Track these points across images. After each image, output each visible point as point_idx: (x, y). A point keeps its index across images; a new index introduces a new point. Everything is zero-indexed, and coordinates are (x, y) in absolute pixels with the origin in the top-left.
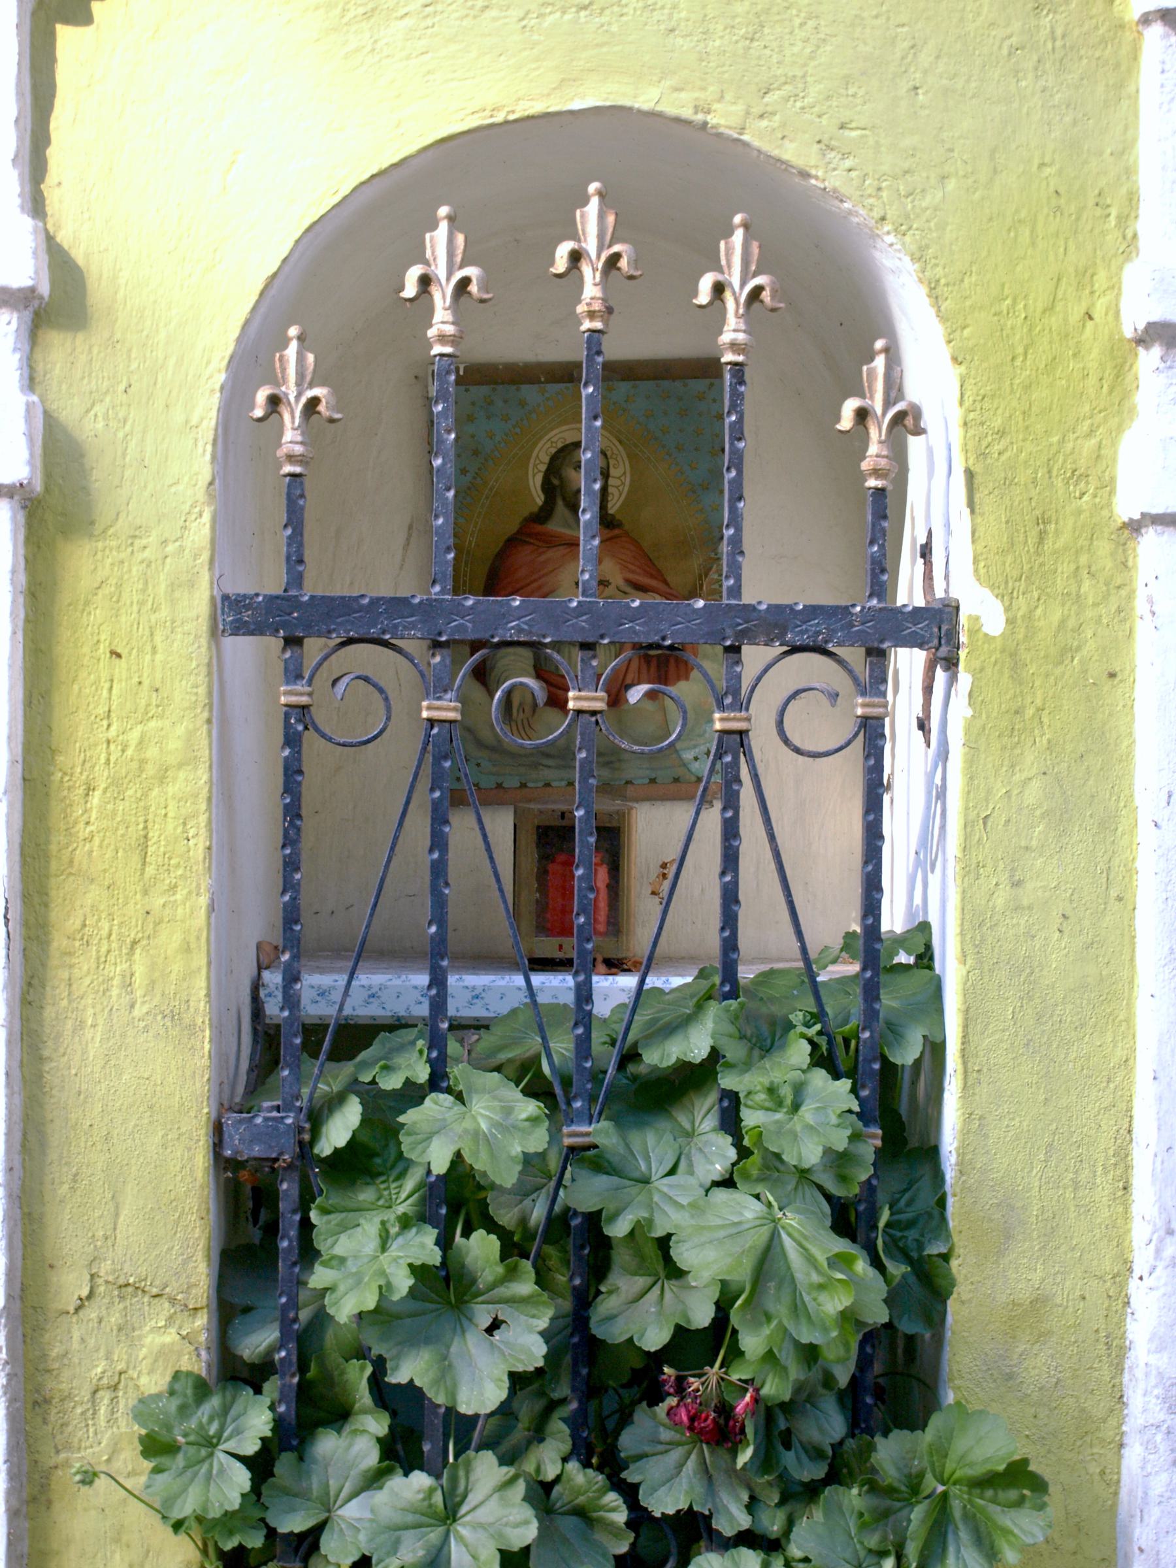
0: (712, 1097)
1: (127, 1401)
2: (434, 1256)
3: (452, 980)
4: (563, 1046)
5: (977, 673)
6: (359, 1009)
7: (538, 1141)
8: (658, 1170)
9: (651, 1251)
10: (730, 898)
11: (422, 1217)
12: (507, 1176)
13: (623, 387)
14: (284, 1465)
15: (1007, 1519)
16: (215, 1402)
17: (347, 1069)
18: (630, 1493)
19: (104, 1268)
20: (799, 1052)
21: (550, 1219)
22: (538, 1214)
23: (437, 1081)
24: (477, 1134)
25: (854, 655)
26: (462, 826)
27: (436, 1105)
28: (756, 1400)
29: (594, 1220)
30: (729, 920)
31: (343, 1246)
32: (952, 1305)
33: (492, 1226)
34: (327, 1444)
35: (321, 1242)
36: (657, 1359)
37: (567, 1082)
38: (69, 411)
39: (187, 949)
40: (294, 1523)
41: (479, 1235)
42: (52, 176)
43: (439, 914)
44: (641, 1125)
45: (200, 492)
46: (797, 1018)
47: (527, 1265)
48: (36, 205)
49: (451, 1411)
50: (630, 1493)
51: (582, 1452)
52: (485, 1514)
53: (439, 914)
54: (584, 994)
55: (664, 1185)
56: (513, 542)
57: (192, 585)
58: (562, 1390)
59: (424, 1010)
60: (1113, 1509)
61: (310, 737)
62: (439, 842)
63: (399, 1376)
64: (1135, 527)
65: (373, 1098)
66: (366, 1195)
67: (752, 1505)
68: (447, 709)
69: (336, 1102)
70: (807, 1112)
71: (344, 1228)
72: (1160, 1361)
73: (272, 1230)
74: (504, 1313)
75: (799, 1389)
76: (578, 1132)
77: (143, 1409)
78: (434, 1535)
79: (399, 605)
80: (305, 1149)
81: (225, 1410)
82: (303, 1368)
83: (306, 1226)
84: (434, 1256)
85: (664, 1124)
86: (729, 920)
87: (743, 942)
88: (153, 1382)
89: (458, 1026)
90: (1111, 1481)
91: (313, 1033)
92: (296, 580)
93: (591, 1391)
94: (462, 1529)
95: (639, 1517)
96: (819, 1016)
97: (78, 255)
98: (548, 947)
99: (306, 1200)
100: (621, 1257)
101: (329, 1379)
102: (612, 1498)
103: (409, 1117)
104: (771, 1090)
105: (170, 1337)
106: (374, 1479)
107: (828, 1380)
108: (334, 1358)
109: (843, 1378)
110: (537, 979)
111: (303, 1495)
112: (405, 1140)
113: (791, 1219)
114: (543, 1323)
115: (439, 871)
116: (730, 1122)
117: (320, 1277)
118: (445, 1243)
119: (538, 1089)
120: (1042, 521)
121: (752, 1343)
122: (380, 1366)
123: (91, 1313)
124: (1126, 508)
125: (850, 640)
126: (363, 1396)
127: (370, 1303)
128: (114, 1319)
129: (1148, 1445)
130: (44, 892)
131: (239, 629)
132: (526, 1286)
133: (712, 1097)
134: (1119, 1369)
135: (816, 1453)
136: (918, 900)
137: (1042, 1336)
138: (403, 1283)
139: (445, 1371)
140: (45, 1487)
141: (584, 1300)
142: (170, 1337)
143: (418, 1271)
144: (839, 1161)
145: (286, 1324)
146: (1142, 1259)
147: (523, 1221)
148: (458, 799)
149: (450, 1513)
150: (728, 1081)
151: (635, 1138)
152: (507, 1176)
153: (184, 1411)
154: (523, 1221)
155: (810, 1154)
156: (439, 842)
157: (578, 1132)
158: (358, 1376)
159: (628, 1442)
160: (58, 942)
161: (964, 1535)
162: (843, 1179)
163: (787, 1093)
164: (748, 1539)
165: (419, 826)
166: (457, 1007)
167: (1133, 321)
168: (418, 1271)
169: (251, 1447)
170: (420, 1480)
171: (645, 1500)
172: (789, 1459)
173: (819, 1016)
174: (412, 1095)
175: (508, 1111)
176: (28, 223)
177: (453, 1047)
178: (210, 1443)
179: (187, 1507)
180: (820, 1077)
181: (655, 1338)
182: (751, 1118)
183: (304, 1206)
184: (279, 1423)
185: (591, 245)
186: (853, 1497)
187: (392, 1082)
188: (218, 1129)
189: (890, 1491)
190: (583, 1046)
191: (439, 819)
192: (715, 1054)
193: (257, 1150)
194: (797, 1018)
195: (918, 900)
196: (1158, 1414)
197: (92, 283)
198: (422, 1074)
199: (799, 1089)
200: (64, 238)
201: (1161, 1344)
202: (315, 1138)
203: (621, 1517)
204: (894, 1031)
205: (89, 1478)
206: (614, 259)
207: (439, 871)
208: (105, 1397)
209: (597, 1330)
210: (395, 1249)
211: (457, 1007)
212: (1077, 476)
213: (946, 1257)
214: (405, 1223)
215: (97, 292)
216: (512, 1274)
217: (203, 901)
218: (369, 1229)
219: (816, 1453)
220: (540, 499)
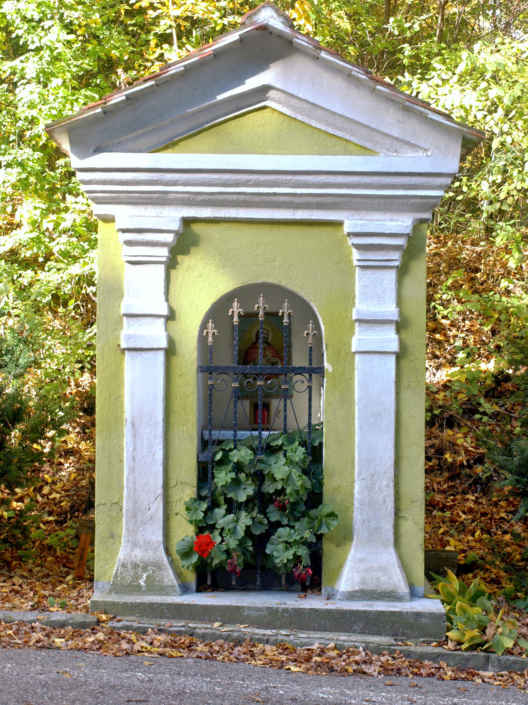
0: (282, 452)
1: (183, 502)
2: (235, 477)
3: (238, 432)
4: (257, 442)
5: (327, 378)
6: (221, 438)
7: (252, 457)
8: (273, 463)
9: (271, 476)
10: (285, 417)
11: (233, 470)
12: (247, 463)
13: (271, 317)
14: (209, 514)
15: (331, 522)
16: (197, 503)
17: (219, 447)
18: (268, 518)
19: (179, 480)
20: (297, 443)
21: (254, 472)
22: (252, 471)
23: (235, 448)
24: (242, 456)
25: (307, 375)
26: (239, 403)
27: (235, 452)
28: (289, 502)
29: (261, 471)
30: (285, 421)
31: (219, 476)
32: (324, 487)
33: (244, 472)
34: (217, 510)
35: (216, 475)
36: (272, 495)
37: (257, 449)
38: (173, 335)
39: (193, 425)
40: (212, 522)
41: (242, 474)
42: (170, 295)
43: (235, 420)
44: (270, 456)
45: (195, 348)
46: (297, 437)
47: (250, 478)
48: (167, 300)
49: (237, 502)
50: (268, 518)
51: (260, 512)
52: (243, 521)
53: (235, 420)
54: (260, 434)
55: (274, 466)
56: (249, 348)
57: (193, 364)
58: (257, 502)
59: (233, 438)
60: (352, 523)
61: (213, 390)
62: (235, 407)
63: (229, 496)
64: (355, 353)
65: (223, 450)
66: (223, 468)
67: (289, 521)
68: (236, 385)
69: (217, 452)
70: (297, 453)
71: (219, 473)
72: (359, 496)
73: (207, 475)
74: (246, 486)
75: (296, 500)
76: (259, 457)
77: (186, 503)
78: (235, 524)
79: (229, 367)
80: (213, 460)
81: (199, 504)
82: (212, 497)
83: (213, 473)
84: (235, 477)
85: (274, 456)
86: (285, 421)
87: (288, 424)
88: (187, 499)
89: (239, 440)
90: (352, 519)
91: (214, 442)
92: (211, 363)
93: (261, 502)
94: (239, 523)
95: (269, 521)
96: (301, 437)
97: (174, 308)
98: (255, 426)
99: (213, 468)
100: (267, 478)
101: (216, 499)
102: (265, 519)
103: (230, 453)
104: (291, 449)
105: (190, 492)
106: (225, 516)
107: (302, 499)
108: (218, 496)
109: (305, 499)
110: (253, 432)
111: (213, 519)
112: (230, 457)
113: (294, 470)
114: (253, 488)
115: (235, 412)
116: (285, 455)
117: (216, 480)
118: (237, 475)
119: (252, 449)
120: (339, 352)
121: (288, 491)
122: (225, 495)
123: (177, 487)
124: (353, 350)
125: (307, 373)
126: (222, 502)
127: (224, 483)
128: (180, 488)
129: (357, 511)
130: (169, 416)
131: (201, 371)
132: (250, 482)
133: (282, 452)
134: (353, 499)
135: (300, 512)
136: (266, 413)
137: (339, 493)
138: (229, 481)
139: (236, 495)
140: (169, 517)
141: (260, 486)
142: (190, 492)
143: (232, 479)
144: (303, 461)
145: (209, 490)
146: (356, 479)
147: (250, 472)
148: (238, 398)
149: (237, 521)
150: (284, 448)
151: (269, 458)
152: (247, 463)
153: (192, 504)
154: (250, 472)
155: (297, 459)
156: (235, 407)
157: (259, 457)
158: (222, 499)
159: (268, 510)
160: (171, 424)
161: (325, 526)
162: (304, 465)
163: (294, 450)
164: (287, 525)
165: (232, 403)
166: (238, 437)
167: (354, 317)
168: (232, 479)
169: (204, 510)
170: (232, 515)
171: (270, 519)
172: (295, 513)
173: (301, 437)
174: (231, 450)
175: (247, 452)
176: (166, 304)
177: (238, 443)
178: (197, 509)
179: (194, 518)
180: (300, 447)
181: (272, 491)
182: (288, 454)
183: (212, 470)
184: (208, 506)
185: (261, 305)
186: (306, 519)
187: (227, 448)
188: (198, 456)
189: (312, 518)
190: (260, 442)
191: (235, 403)
192: (282, 444)
193: (205, 460)
194: (297, 437)
195: (266, 413)
196: (359, 506)
197: (176, 313)
198: (233, 447)
199: (296, 449)
200: (172, 305)
201: (359, 493)
202: (214, 457)
203: (266, 522)
204: (314, 440)
205: (177, 514)
206: (265, 308)
207: (235, 412)
208: (179, 502)
209: (262, 490)
210: (228, 476)
211: (238, 437)
212: (345, 344)
213: (323, 479)
214: (230, 472)
215: (177, 315)
216: (248, 480)
217: (196, 417)
218: (224, 473)
219: (300, 512)
220: (255, 340)
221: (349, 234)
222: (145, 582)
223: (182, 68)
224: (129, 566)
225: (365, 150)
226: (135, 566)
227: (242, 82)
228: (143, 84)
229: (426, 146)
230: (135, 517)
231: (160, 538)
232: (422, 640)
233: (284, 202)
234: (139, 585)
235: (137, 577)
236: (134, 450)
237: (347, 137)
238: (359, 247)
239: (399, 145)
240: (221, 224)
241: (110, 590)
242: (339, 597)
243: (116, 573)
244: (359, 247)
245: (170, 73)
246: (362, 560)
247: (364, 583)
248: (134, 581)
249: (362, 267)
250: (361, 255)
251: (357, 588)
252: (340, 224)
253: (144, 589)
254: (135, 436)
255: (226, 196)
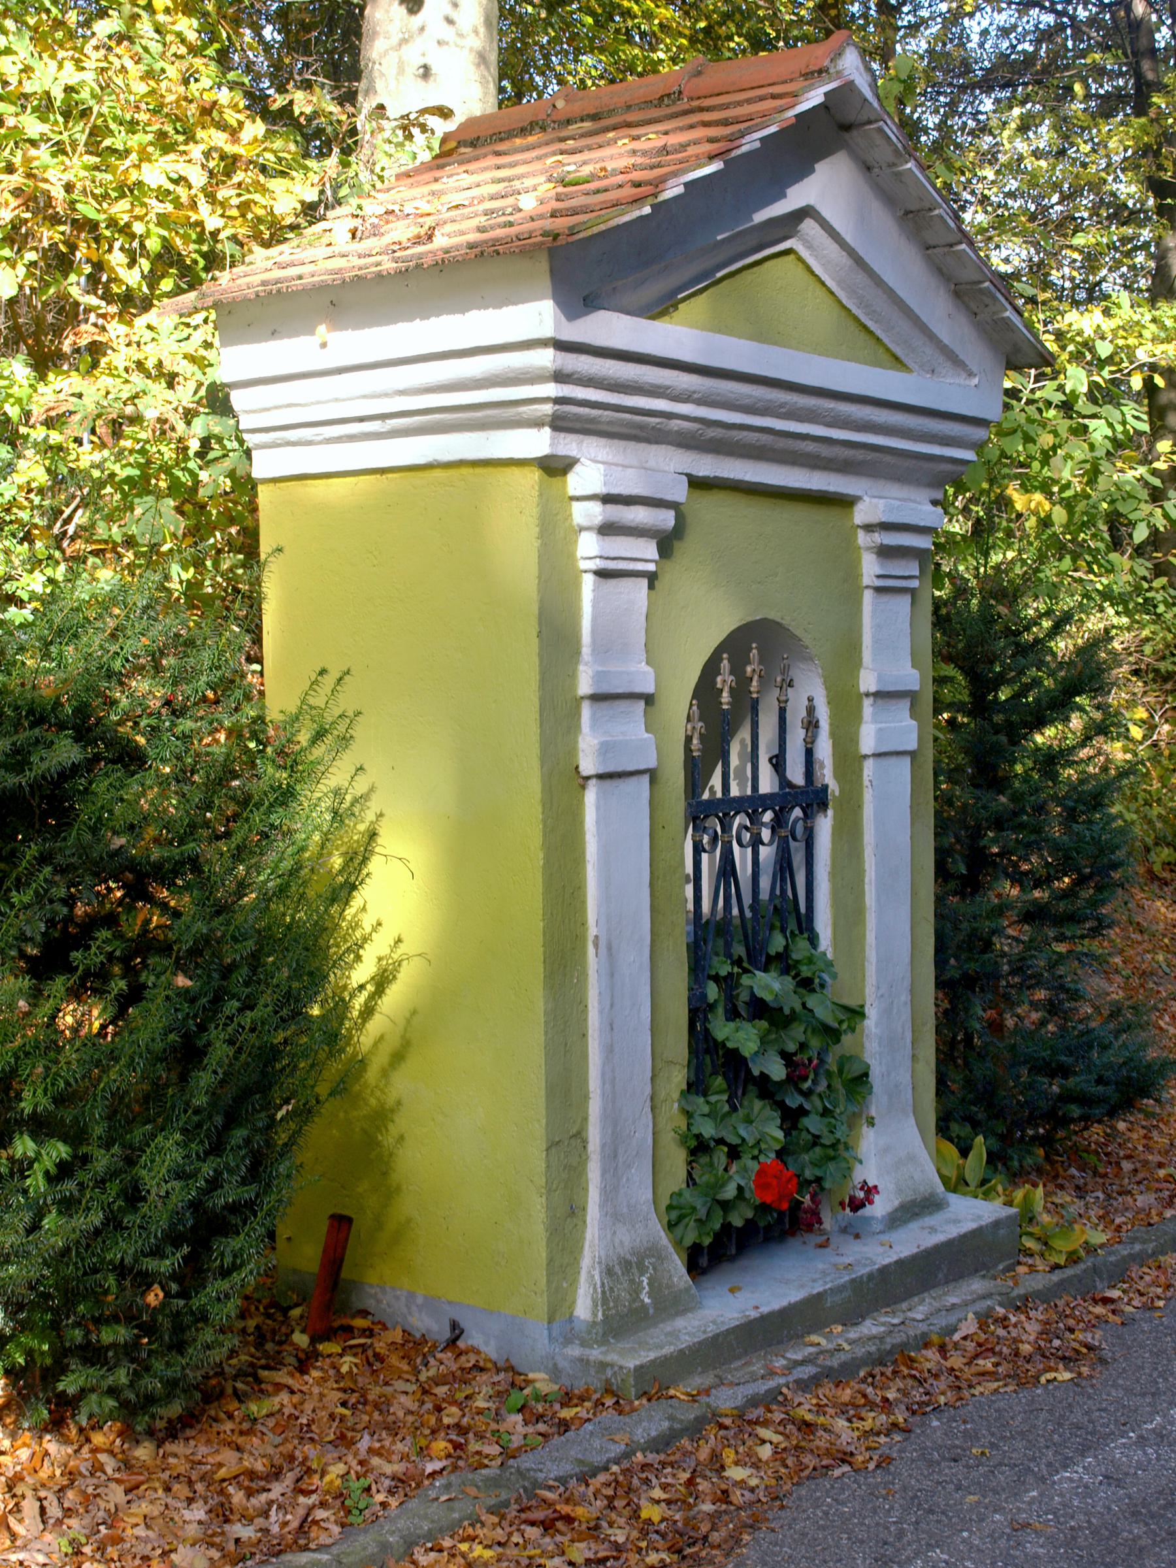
221: (869, 528)
222: (650, 1295)
223: (757, 145)
224: (617, 1269)
225: (897, 362)
226: (626, 1265)
227: (782, 195)
228: (704, 165)
229: (975, 369)
230: (615, 1156)
231: (650, 1195)
232: (1001, 1267)
233: (808, 455)
234: (644, 1307)
235: (636, 1291)
236: (612, 1006)
237: (879, 333)
238: (885, 552)
239: (941, 359)
240: (715, 491)
241: (604, 1334)
242: (877, 1227)
243: (603, 1292)
244: (885, 552)
245: (744, 149)
246: (886, 1150)
247: (900, 1191)
248: (634, 1301)
249: (879, 590)
250: (882, 566)
251: (896, 1203)
252: (846, 502)
253: (651, 1311)
254: (612, 975)
255: (745, 433)
